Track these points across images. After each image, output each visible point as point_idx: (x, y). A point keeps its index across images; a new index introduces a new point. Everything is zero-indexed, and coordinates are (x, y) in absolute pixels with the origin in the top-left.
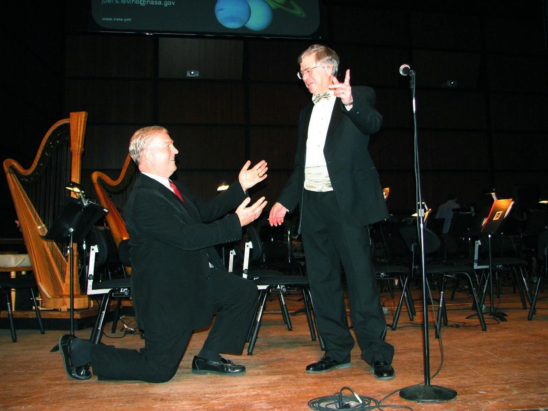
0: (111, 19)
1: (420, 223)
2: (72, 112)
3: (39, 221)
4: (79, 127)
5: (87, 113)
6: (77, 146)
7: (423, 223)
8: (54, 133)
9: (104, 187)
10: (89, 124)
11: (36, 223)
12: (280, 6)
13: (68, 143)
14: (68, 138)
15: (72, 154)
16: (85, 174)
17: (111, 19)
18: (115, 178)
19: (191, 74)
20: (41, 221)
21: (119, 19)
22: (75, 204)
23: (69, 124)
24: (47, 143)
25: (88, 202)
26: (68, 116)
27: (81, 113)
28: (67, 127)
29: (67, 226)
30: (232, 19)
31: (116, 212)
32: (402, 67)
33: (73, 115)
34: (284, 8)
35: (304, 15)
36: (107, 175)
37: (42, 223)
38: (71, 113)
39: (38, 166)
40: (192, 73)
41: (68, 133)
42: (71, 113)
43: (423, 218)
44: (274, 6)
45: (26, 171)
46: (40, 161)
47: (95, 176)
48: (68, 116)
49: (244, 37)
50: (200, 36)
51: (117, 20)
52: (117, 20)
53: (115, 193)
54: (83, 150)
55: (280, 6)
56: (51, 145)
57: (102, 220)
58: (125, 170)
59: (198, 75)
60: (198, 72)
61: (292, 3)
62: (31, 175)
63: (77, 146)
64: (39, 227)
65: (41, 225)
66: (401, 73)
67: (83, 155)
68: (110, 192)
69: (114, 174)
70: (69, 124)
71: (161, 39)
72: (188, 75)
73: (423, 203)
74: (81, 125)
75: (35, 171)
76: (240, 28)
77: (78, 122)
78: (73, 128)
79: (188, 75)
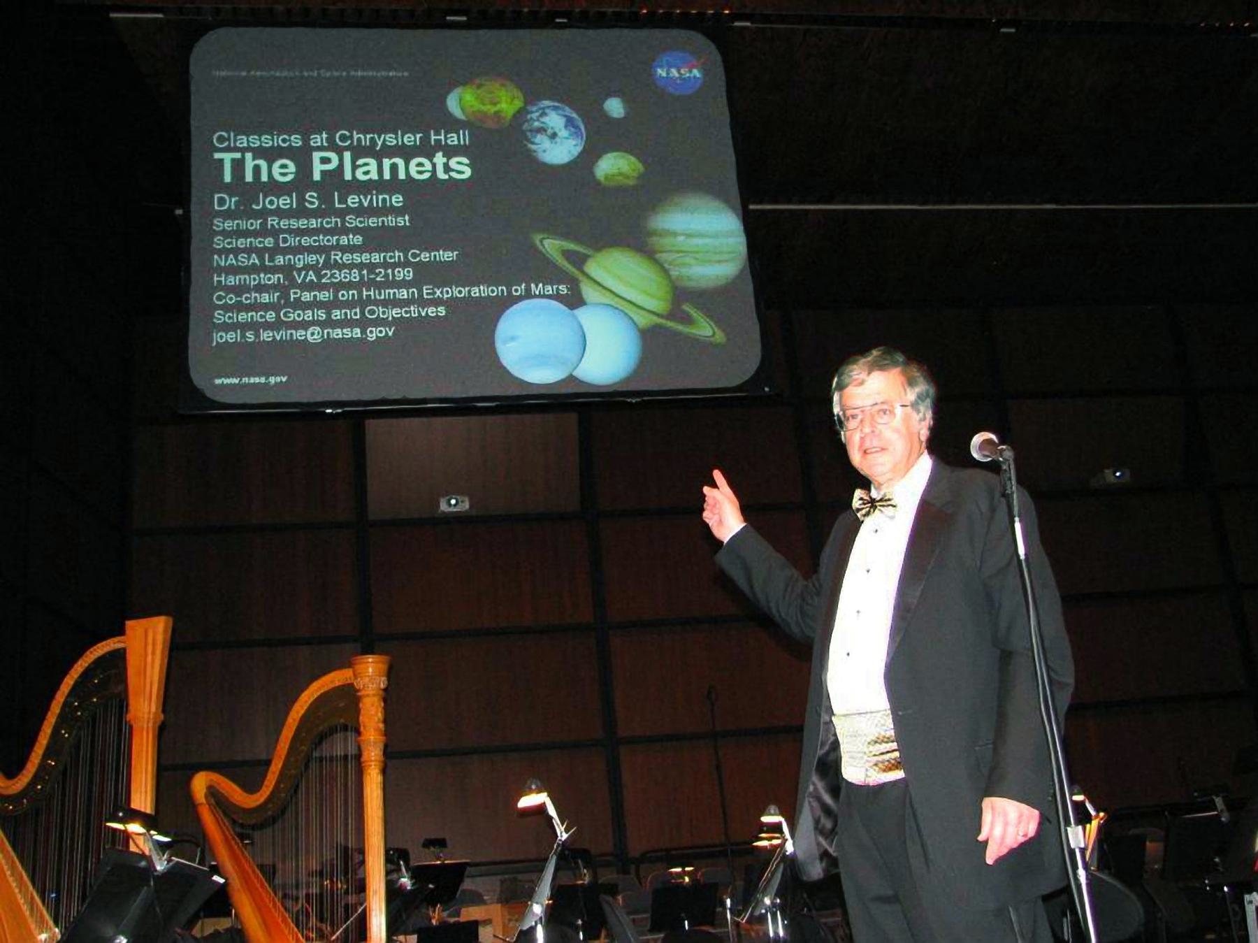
0: (236, 381)
1: (1075, 868)
2: (130, 619)
3: (42, 916)
4: (149, 658)
5: (171, 620)
6: (145, 708)
7: (1086, 867)
8: (86, 674)
9: (225, 813)
10: (176, 648)
11: (33, 926)
12: (660, 321)
13: (122, 704)
14: (120, 688)
15: (131, 727)
16: (171, 779)
17: (236, 381)
18: (251, 786)
19: (450, 505)
20: (47, 917)
21: (257, 380)
22: (133, 872)
23: (124, 649)
24: (65, 705)
25: (169, 861)
26: (121, 632)
27: (156, 619)
28: (117, 659)
29: (109, 931)
30: (541, 360)
31: (258, 878)
32: (977, 439)
33: (135, 627)
34: (670, 324)
35: (720, 337)
36: (234, 781)
37: (51, 923)
38: (129, 623)
39: (43, 767)
40: (453, 502)
41: (122, 678)
42: (129, 623)
43: (1083, 851)
44: (644, 320)
45: (10, 783)
46: (48, 754)
47: (200, 783)
48: (121, 632)
49: (576, 405)
50: (463, 407)
51: (252, 380)
52: (252, 380)
53: (253, 827)
54: (162, 717)
55: (660, 321)
56: (77, 709)
57: (220, 902)
58: (280, 766)
59: (466, 506)
60: (467, 500)
61: (687, 307)
62: (24, 793)
63: (145, 708)
64: (43, 936)
65: (48, 929)
66: (975, 455)
67: (162, 731)
68: (242, 826)
69: (248, 772)
70: (124, 649)
71: (372, 425)
72: (443, 507)
73: (1079, 798)
74: (153, 653)
75: (36, 778)
76: (563, 381)
77: (146, 644)
78: (133, 662)
79: (443, 507)
